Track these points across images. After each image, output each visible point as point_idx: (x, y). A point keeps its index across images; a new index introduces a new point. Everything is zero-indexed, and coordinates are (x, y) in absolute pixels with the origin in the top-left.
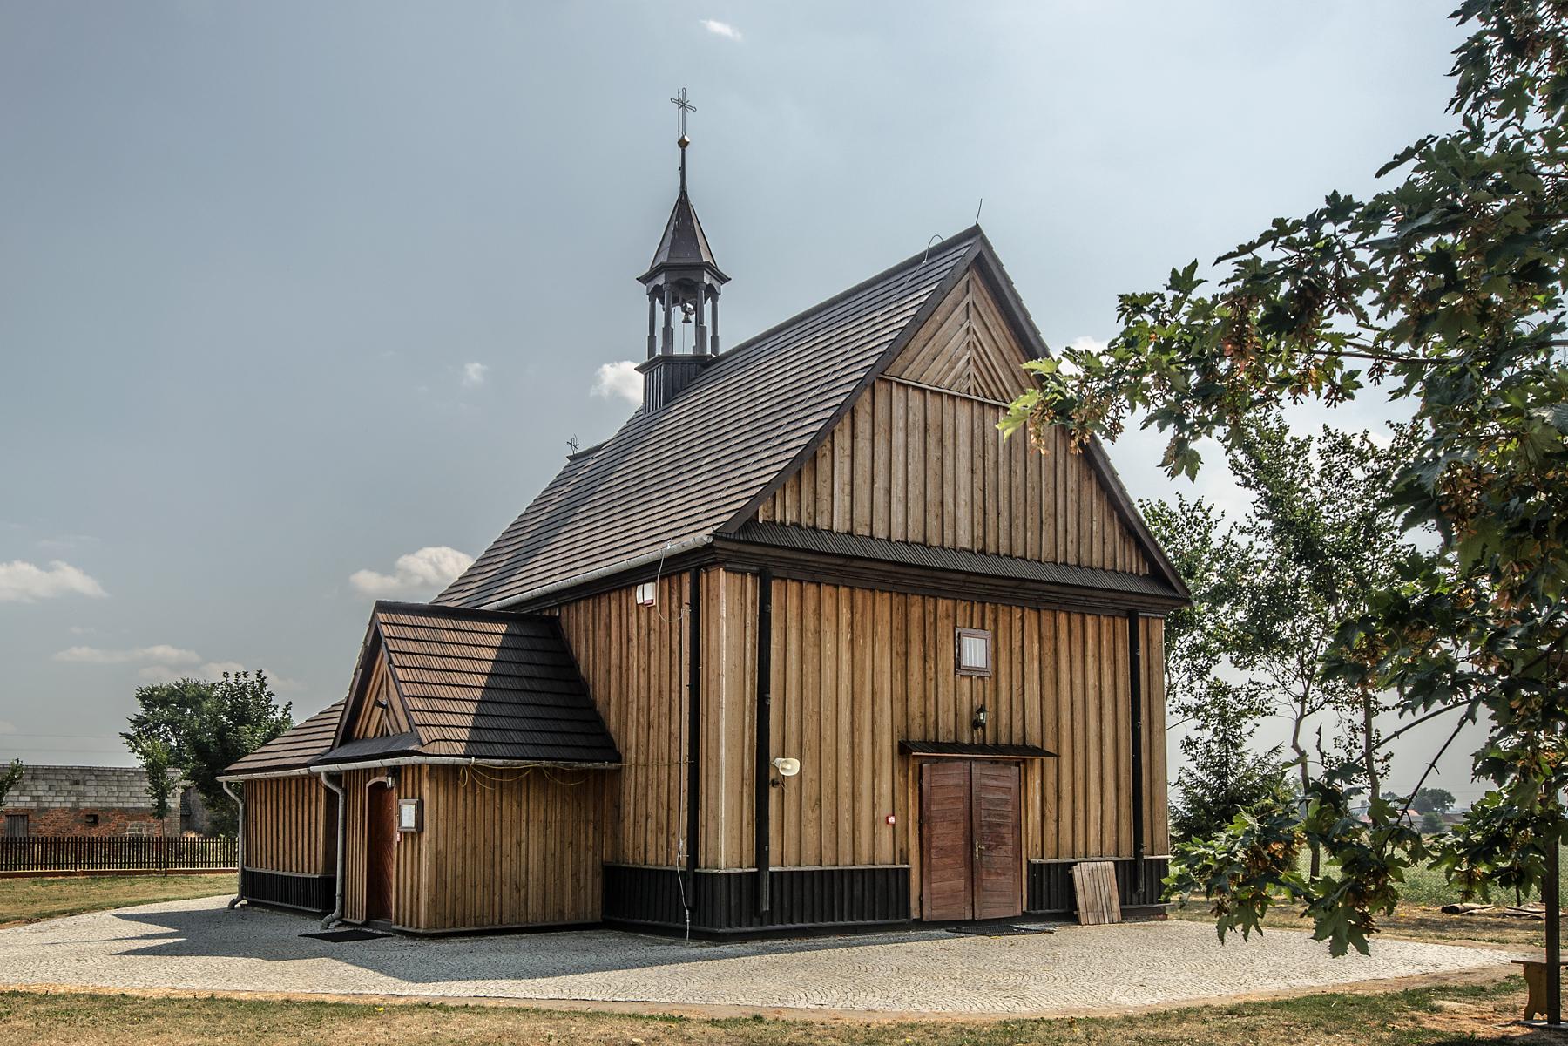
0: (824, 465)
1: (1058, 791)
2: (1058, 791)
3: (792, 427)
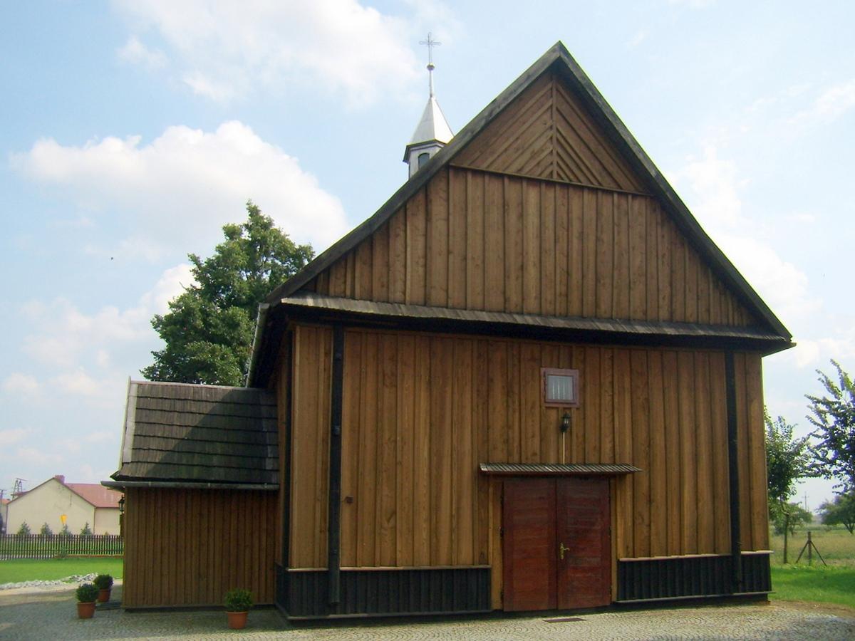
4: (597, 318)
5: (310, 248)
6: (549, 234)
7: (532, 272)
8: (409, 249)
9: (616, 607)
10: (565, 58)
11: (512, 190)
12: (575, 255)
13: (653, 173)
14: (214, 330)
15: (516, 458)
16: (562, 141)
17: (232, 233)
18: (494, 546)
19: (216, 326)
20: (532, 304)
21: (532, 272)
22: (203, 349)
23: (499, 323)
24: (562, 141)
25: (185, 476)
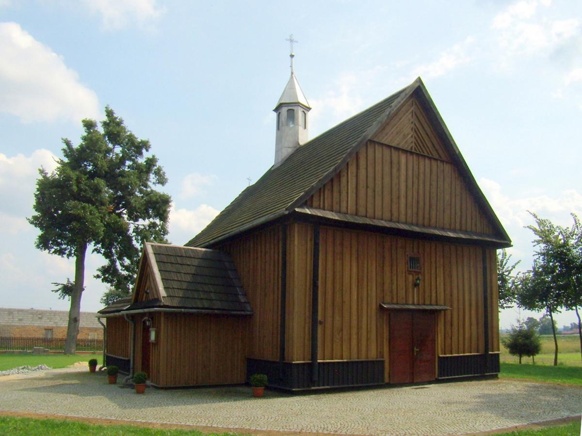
0: (344, 180)
1: (418, 192)
2: (418, 192)
3: (331, 162)
4: (429, 226)
5: (148, 142)
6: (410, 181)
7: (403, 201)
8: (349, 184)
9: (438, 381)
10: (421, 86)
11: (395, 154)
12: (421, 192)
13: (457, 152)
14: (84, 194)
15: (395, 301)
16: (416, 130)
17: (89, 125)
18: (386, 349)
19: (85, 191)
20: (402, 218)
21: (403, 201)
22: (77, 206)
23: (370, 225)
24: (416, 130)
25: (200, 306)
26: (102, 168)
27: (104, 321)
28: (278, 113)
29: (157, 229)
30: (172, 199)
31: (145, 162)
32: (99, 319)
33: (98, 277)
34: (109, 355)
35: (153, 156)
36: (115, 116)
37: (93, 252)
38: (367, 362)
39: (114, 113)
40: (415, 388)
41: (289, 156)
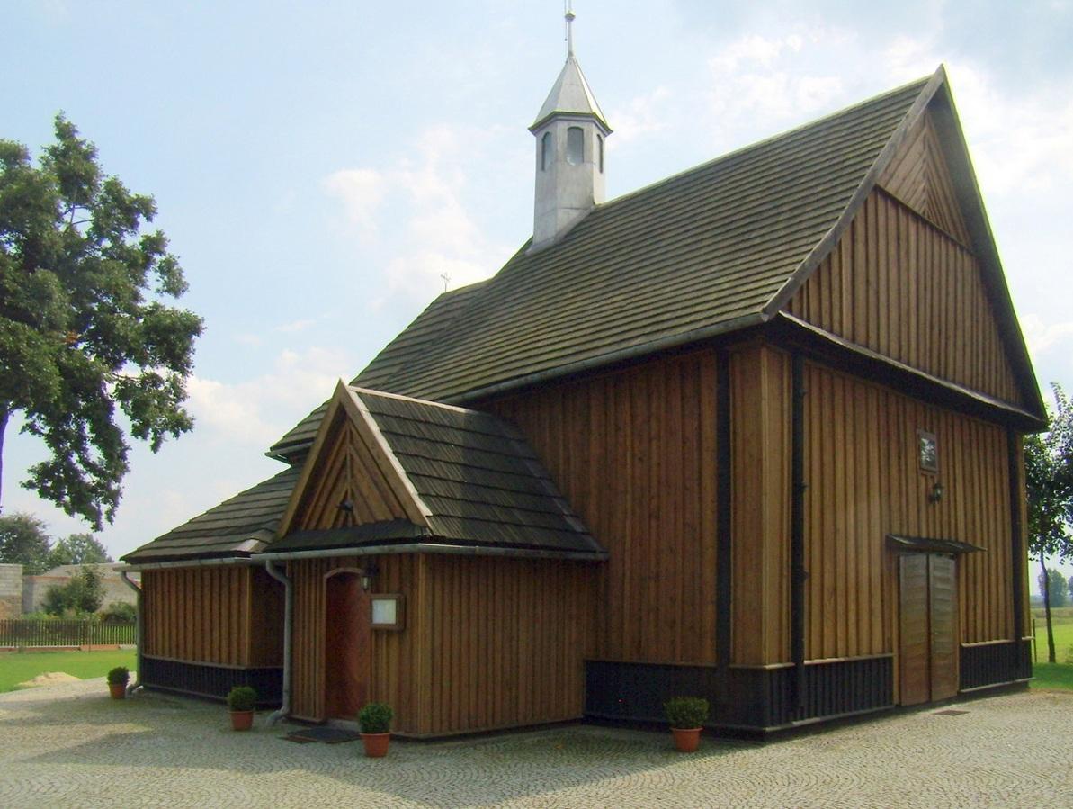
19: (15, 294)
25: (518, 539)
26: (51, 247)
27: (137, 579)
28: (542, 135)
29: (161, 388)
30: (203, 325)
31: (141, 244)
32: (124, 574)
33: (30, 485)
34: (148, 656)
35: (159, 233)
36: (79, 137)
37: (24, 430)
38: (870, 661)
39: (77, 132)
40: (940, 713)
41: (571, 227)
